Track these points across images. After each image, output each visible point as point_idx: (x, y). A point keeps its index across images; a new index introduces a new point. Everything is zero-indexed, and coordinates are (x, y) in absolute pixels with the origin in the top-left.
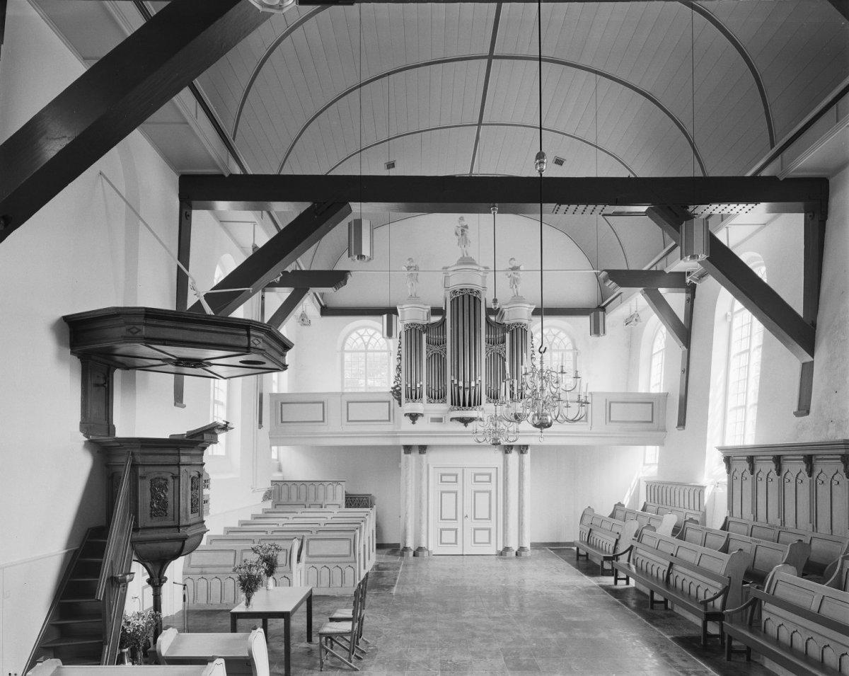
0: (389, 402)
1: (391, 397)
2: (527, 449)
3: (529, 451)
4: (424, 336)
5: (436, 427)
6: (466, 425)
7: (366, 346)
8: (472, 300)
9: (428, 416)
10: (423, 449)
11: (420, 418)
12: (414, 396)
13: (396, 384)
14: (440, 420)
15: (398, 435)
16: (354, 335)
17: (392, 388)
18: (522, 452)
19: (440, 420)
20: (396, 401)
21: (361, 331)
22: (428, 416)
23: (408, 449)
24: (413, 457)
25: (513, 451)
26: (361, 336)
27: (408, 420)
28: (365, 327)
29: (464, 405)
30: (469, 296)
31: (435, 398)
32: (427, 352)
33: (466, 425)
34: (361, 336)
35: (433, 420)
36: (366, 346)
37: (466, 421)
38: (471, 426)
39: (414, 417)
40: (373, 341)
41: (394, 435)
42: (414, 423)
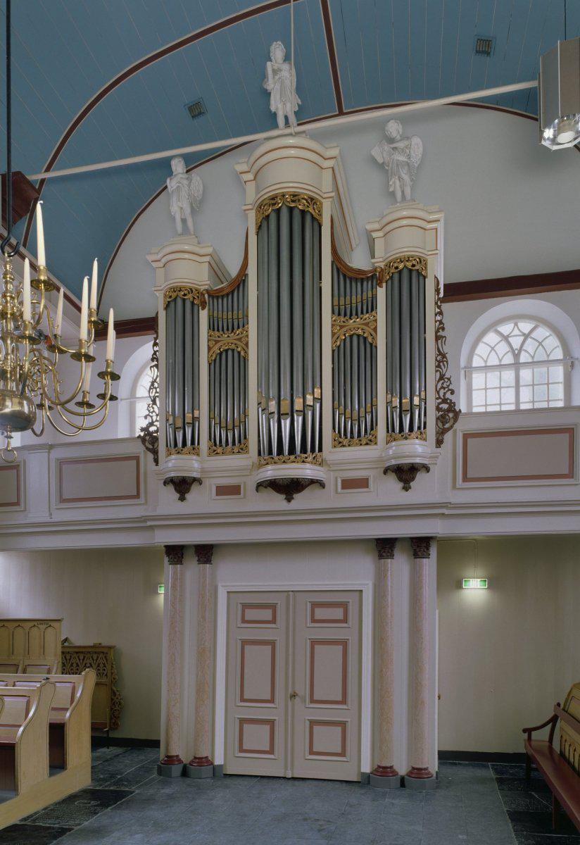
0: (137, 459)
1: (139, 449)
2: (428, 547)
3: (433, 551)
4: (204, 315)
5: (228, 505)
6: (289, 500)
7: (516, 356)
8: (297, 215)
9: (211, 484)
10: (205, 553)
11: (195, 488)
12: (187, 445)
13: (149, 420)
14: (233, 490)
15: (149, 523)
16: (491, 338)
17: (142, 430)
18: (416, 555)
19: (233, 490)
20: (150, 456)
21: (506, 329)
22: (211, 484)
23: (176, 553)
24: (191, 569)
25: (397, 553)
26: (506, 338)
27: (170, 493)
28: (516, 318)
29: (280, 451)
30: (184, 300)
31: (352, 437)
32: (209, 349)
33: (289, 500)
34: (506, 338)
35: (223, 491)
36: (516, 356)
37: (290, 488)
38: (302, 501)
39: (182, 485)
40: (530, 346)
41: (142, 525)
42: (182, 499)
